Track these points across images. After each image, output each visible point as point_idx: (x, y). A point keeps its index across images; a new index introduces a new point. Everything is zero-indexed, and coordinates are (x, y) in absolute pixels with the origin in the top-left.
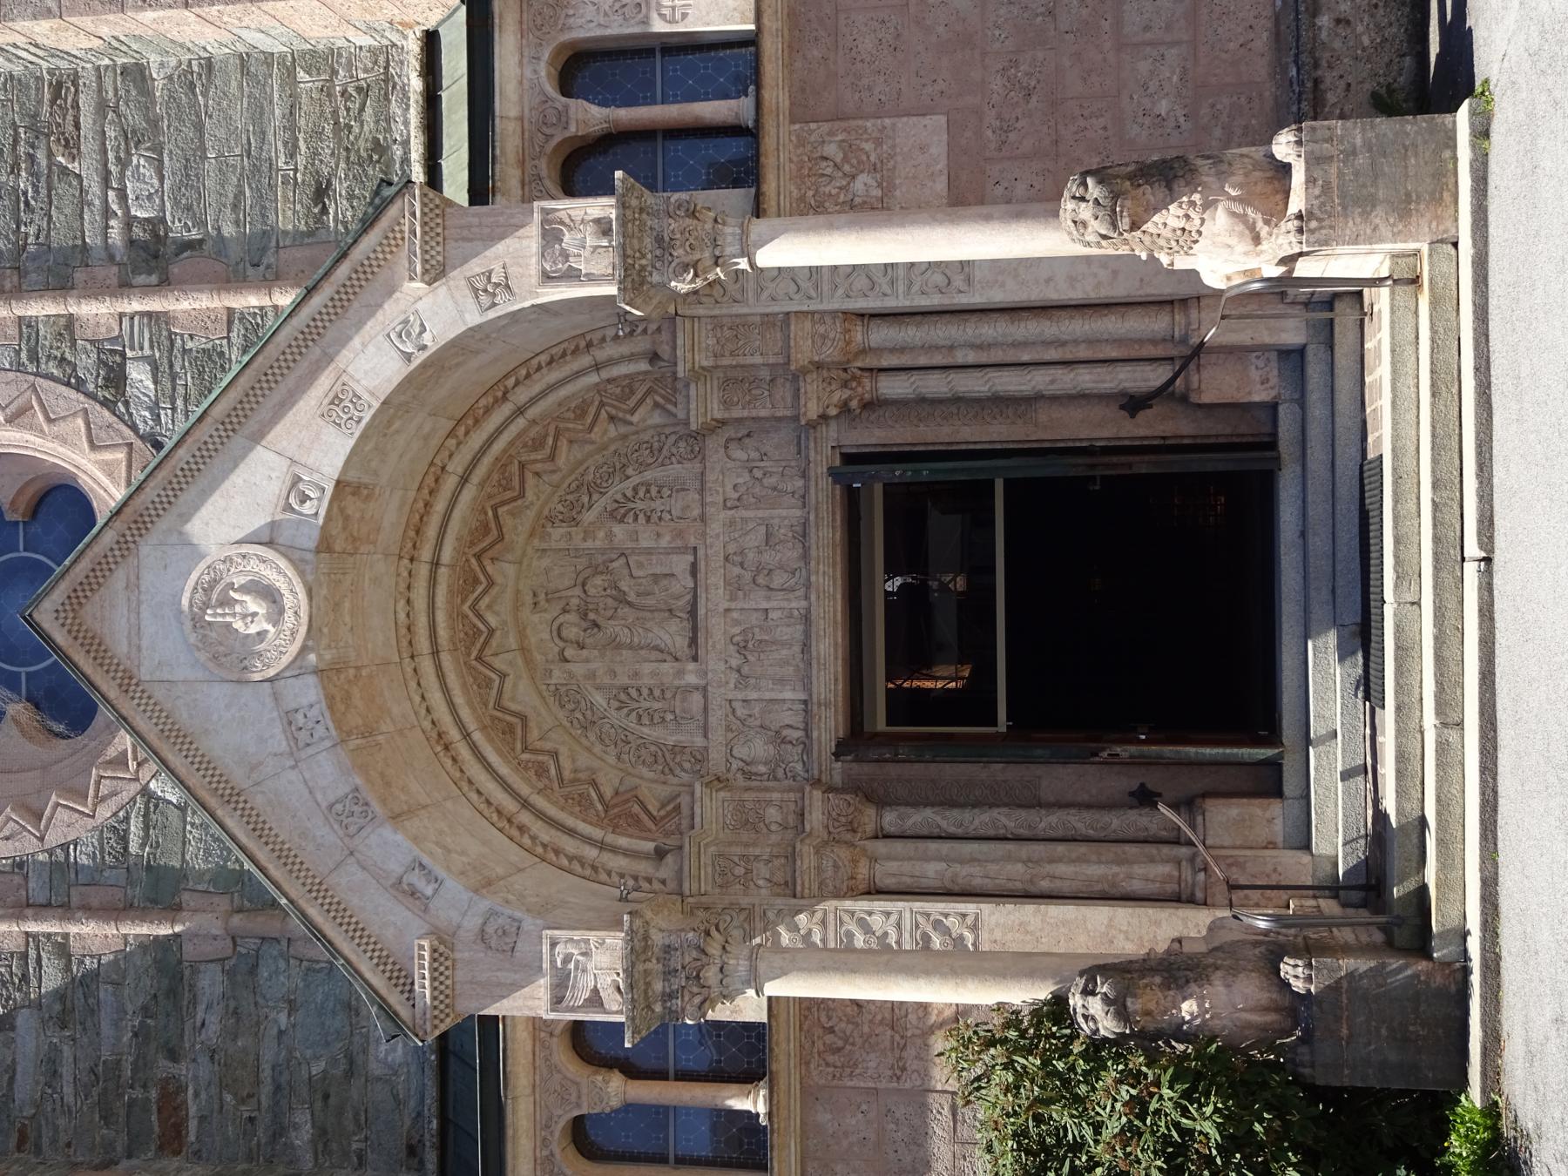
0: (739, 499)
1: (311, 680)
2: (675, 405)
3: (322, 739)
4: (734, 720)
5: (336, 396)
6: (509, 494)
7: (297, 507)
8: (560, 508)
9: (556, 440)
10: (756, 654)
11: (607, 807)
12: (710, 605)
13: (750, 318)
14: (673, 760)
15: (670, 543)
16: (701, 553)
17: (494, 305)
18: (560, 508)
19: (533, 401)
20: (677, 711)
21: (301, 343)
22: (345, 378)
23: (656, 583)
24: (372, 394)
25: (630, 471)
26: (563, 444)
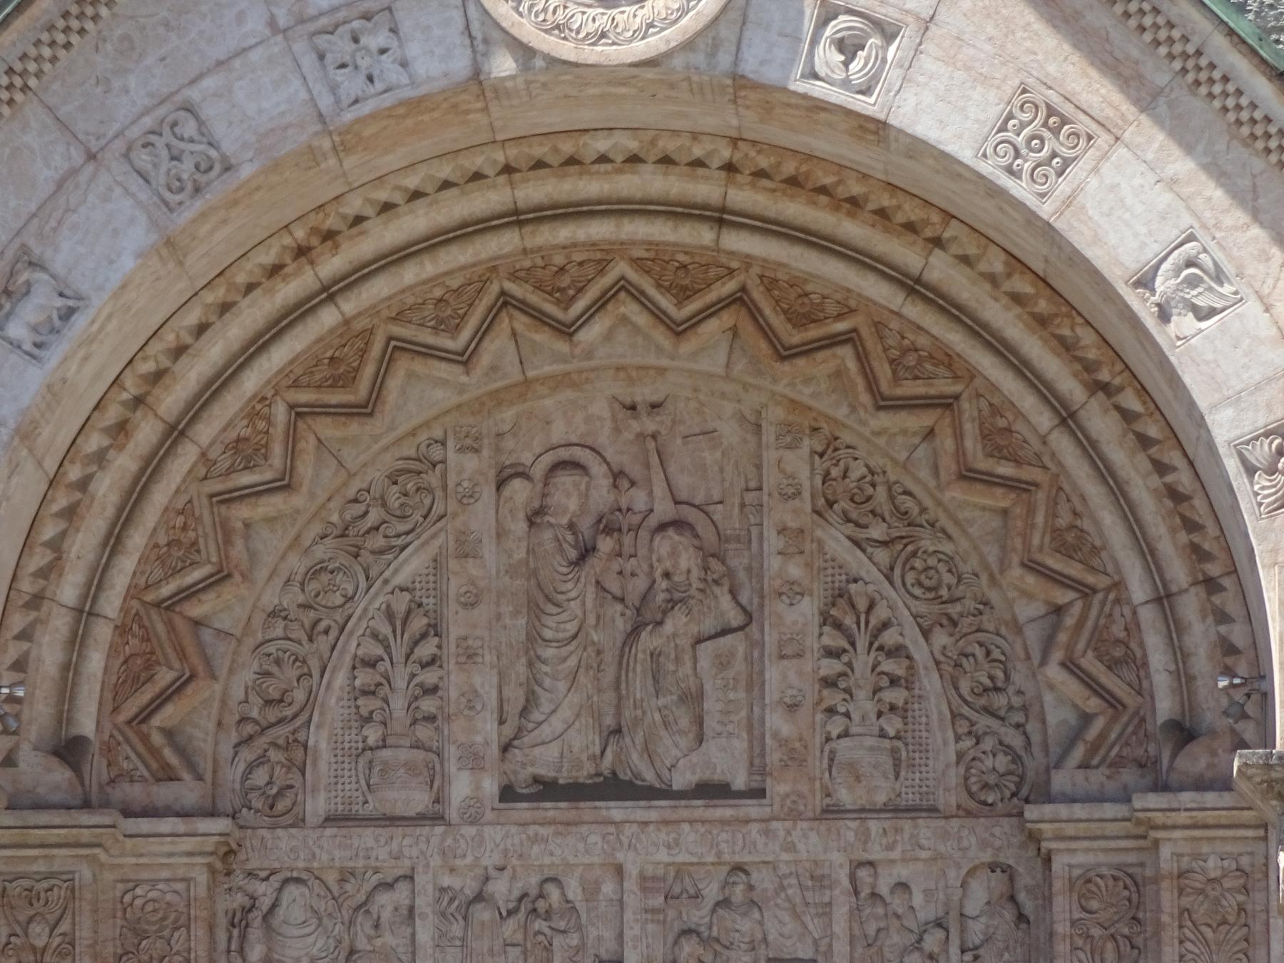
0: (874, 895)
1: (460, 65)
2: (1084, 766)
3: (333, 89)
4: (368, 887)
5: (1064, 121)
6: (883, 371)
7: (829, 31)
8: (858, 471)
9: (1010, 484)
10: (519, 937)
11: (168, 606)
12: (629, 830)
13: (1261, 952)
14: (274, 744)
15: (775, 735)
16: (751, 808)
17: (1251, 470)
18: (858, 471)
19: (1090, 448)
20: (386, 754)
21: (1178, 48)
22: (1103, 139)
23: (684, 698)
24: (1069, 201)
25: (941, 638)
26: (1001, 499)
